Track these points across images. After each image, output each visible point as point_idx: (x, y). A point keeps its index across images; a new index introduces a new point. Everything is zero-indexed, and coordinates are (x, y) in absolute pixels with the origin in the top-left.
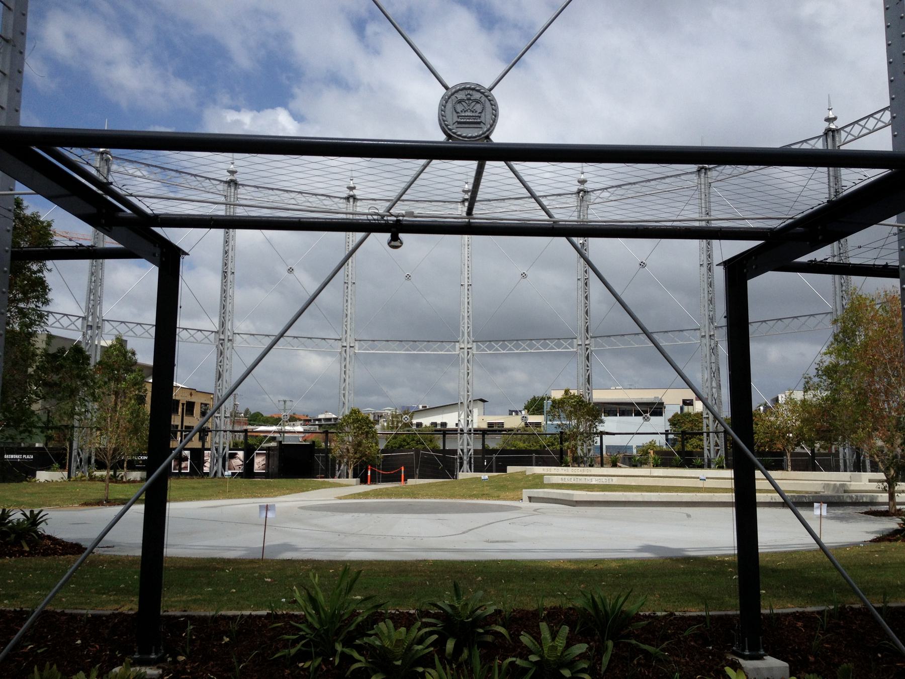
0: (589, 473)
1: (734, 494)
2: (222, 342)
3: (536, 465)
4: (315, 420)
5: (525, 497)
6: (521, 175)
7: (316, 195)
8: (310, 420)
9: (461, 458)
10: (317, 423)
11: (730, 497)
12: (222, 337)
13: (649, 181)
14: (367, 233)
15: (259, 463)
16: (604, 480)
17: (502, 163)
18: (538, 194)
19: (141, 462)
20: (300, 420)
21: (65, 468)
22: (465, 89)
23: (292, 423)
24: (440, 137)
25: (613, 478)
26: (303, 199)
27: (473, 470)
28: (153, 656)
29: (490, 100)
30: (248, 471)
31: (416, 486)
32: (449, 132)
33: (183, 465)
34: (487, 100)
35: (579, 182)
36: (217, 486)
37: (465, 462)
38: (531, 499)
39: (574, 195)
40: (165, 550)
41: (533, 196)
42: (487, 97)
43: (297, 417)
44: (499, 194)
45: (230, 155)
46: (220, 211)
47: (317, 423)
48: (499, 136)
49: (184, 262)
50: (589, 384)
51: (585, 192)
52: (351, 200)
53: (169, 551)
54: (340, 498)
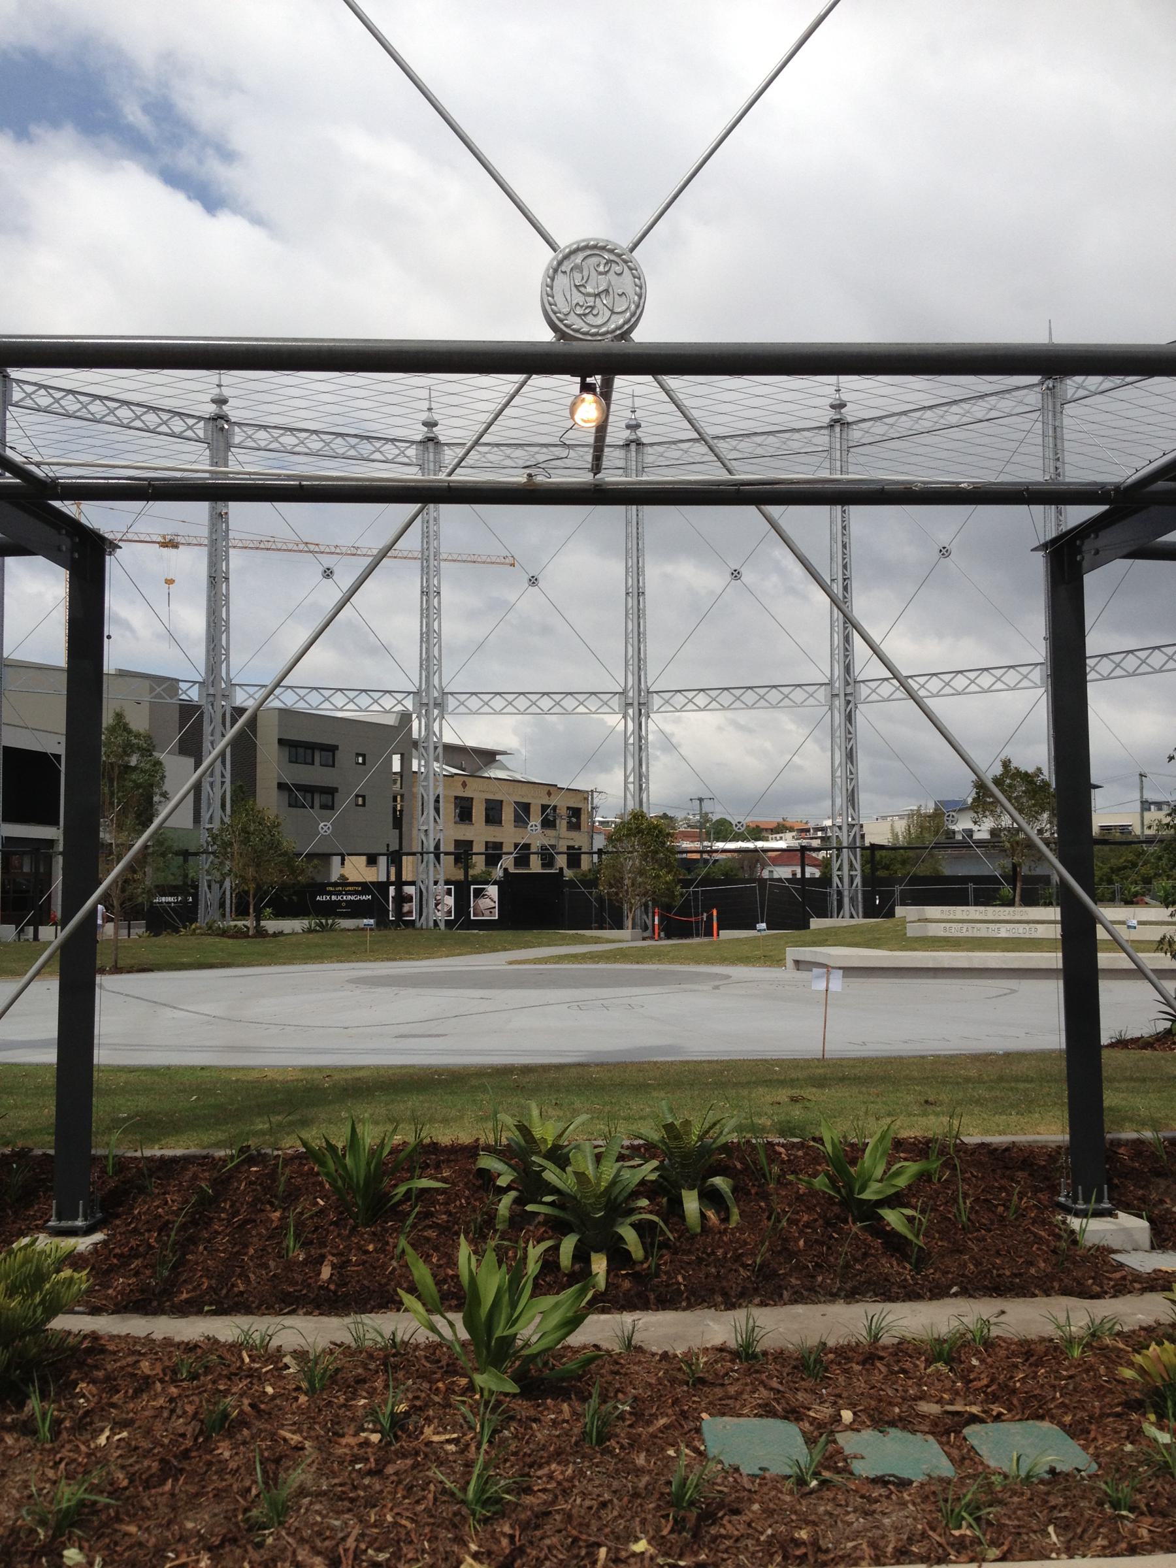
0: (1024, 918)
1: (1060, 955)
2: (211, 699)
3: (976, 904)
4: (817, 829)
5: (789, 963)
6: (681, 396)
7: (674, 443)
8: (808, 830)
9: (840, 893)
10: (820, 834)
11: (1055, 959)
12: (211, 691)
13: (955, 402)
14: (419, 505)
15: (489, 901)
16: (1021, 931)
17: (649, 378)
18: (711, 431)
19: (344, 904)
20: (791, 830)
21: (248, 914)
22: (587, 247)
23: (778, 836)
24: (546, 335)
25: (1038, 926)
26: (369, 446)
27: (861, 914)
28: (79, 1223)
29: (631, 269)
30: (462, 919)
31: (730, 941)
32: (557, 322)
33: (406, 908)
34: (626, 269)
35: (832, 406)
36: (333, 946)
37: (846, 900)
38: (797, 963)
39: (822, 432)
40: (96, 1052)
41: (702, 438)
42: (626, 262)
43: (788, 825)
44: (503, 433)
45: (832, 379)
46: (411, 474)
47: (820, 834)
48: (647, 334)
49: (113, 566)
50: (852, 763)
51: (638, 444)
52: (633, 447)
53: (102, 1056)
54: (510, 963)
